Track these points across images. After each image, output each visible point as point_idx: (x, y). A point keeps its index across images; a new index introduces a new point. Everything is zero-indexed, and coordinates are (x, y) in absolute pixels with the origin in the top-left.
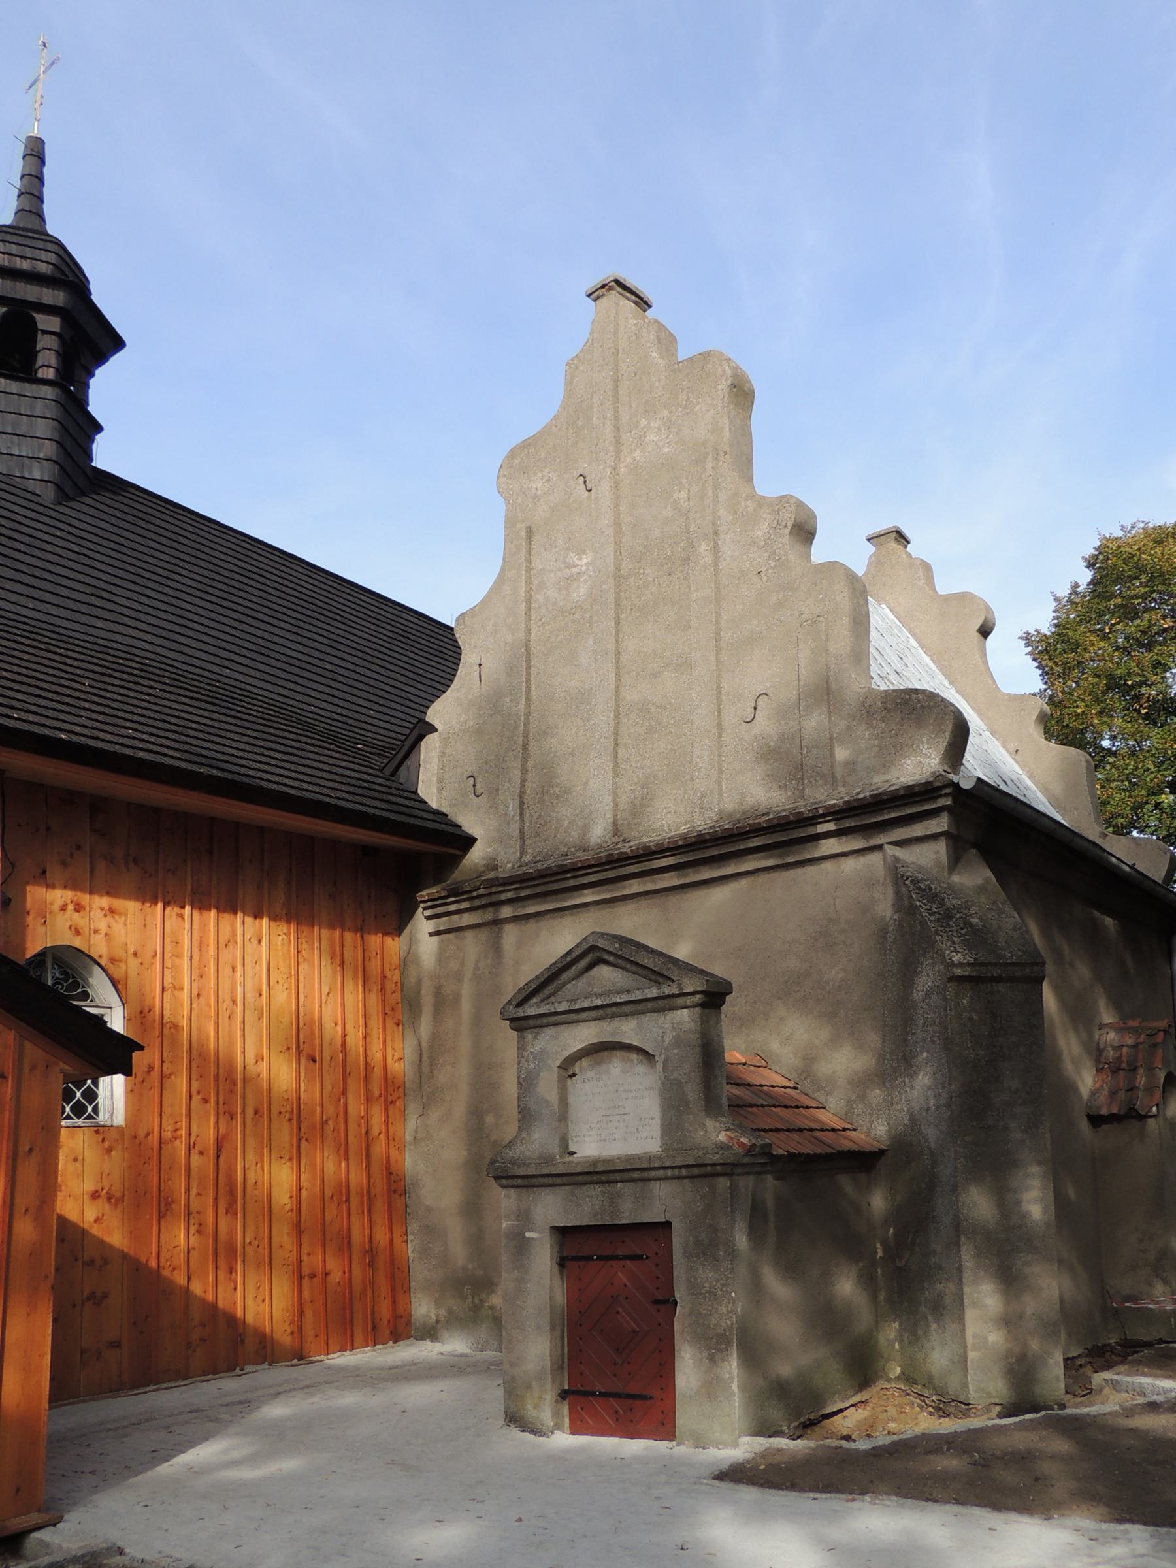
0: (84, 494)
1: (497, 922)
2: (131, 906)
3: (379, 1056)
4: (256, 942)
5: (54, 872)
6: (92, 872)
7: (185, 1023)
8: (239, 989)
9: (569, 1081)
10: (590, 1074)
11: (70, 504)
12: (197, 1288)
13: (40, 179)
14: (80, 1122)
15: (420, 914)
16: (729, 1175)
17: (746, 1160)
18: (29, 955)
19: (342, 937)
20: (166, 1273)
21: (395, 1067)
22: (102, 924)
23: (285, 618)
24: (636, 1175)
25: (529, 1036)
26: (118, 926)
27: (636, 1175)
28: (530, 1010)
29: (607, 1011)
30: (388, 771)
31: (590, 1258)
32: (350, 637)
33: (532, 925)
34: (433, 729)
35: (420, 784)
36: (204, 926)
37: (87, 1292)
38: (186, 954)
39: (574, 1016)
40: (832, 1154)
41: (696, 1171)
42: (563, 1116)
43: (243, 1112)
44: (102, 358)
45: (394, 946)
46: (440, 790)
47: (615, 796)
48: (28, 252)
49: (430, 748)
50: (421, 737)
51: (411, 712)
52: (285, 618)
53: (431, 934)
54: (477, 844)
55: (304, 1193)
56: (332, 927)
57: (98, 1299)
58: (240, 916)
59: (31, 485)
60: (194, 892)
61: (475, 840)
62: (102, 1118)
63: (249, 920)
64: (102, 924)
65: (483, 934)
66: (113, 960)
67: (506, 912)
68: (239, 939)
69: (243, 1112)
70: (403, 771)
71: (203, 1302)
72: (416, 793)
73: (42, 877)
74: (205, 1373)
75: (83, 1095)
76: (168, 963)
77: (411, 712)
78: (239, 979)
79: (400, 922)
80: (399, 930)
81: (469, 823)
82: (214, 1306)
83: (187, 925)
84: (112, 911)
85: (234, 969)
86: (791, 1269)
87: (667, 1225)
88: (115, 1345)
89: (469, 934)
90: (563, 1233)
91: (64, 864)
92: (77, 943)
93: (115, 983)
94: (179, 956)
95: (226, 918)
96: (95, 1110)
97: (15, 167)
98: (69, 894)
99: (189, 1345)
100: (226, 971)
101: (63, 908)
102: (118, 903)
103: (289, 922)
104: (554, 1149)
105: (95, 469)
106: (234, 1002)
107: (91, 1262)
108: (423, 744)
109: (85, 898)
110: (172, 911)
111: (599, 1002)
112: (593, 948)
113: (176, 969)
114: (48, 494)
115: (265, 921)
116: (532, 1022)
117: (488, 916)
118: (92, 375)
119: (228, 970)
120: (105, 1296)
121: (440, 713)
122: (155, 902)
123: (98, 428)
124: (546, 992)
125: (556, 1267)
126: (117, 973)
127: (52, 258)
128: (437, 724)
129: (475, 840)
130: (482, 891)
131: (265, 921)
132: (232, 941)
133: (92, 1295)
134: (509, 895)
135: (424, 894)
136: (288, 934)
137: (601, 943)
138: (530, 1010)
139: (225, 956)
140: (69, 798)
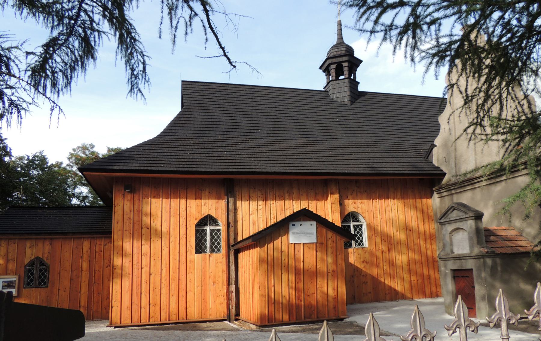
0: (357, 100)
1: (452, 194)
2: (366, 201)
3: (428, 228)
4: (394, 205)
5: (350, 197)
6: (357, 196)
7: (379, 225)
8: (391, 216)
9: (452, 237)
10: (456, 235)
11: (354, 104)
12: (386, 282)
13: (341, 30)
14: (359, 247)
15: (435, 193)
16: (483, 258)
17: (487, 255)
18: (346, 214)
19: (416, 201)
20: (379, 279)
21: (432, 231)
22: (360, 206)
23: (406, 116)
24: (465, 258)
25: (443, 226)
26: (363, 206)
27: (465, 258)
28: (442, 221)
29: (455, 221)
30: (426, 158)
31: (459, 277)
32: (426, 115)
33: (459, 195)
34: (436, 146)
35: (433, 160)
36: (382, 203)
37: (363, 281)
38: (378, 210)
39: (450, 222)
40: (519, 253)
41: (476, 257)
42: (451, 244)
43: (394, 243)
44: (358, 66)
45: (430, 201)
46: (438, 161)
47: (476, 160)
48: (340, 49)
49: (435, 150)
50: (432, 149)
51: (427, 143)
52: (406, 116)
53: (438, 198)
54: (447, 175)
55: (410, 261)
56: (413, 199)
57: (366, 283)
58: (390, 200)
59: (345, 103)
60: (379, 196)
61: (446, 174)
62: (364, 246)
63: (392, 200)
64: (360, 206)
65: (449, 197)
66: (363, 213)
67: (453, 192)
68: (390, 205)
69: (394, 243)
70: (429, 158)
71: (388, 286)
72: (432, 163)
73: (347, 198)
74: (389, 300)
75: (44, 277)
76: (374, 212)
77: (427, 143)
78: (391, 214)
79: (431, 196)
80: (431, 197)
81: (444, 169)
82: (391, 287)
83: (378, 203)
84: (362, 203)
85: (389, 212)
86: (505, 282)
87: (472, 269)
88: (370, 293)
89: (446, 198)
90: (454, 271)
91: (351, 195)
92: (355, 210)
93: (364, 218)
94: (377, 210)
95: (387, 200)
96: (363, 244)
97: (335, 28)
98: (353, 200)
99: (386, 294)
100: (387, 212)
101: (352, 204)
102: (363, 201)
103: (402, 199)
104: (449, 252)
105: (360, 92)
106: (390, 219)
107: (363, 276)
108: (433, 150)
109: (356, 201)
110: (374, 201)
111: (455, 219)
112: (453, 207)
113: (376, 213)
114: (349, 103)
115: (396, 200)
116: (443, 223)
117: (449, 193)
118: (356, 71)
119: (388, 212)
120: (367, 282)
121: (438, 141)
122: (370, 199)
123: (359, 83)
124: (445, 216)
125: (453, 279)
126: (364, 215)
127: (345, 49)
128: (437, 144)
129: (446, 174)
130: (447, 187)
131: (396, 200)
132: (388, 205)
133: (364, 282)
134: (453, 188)
135: (434, 189)
136: (402, 202)
137: (454, 205)
138: (442, 221)
139: (387, 209)
140: (351, 181)
